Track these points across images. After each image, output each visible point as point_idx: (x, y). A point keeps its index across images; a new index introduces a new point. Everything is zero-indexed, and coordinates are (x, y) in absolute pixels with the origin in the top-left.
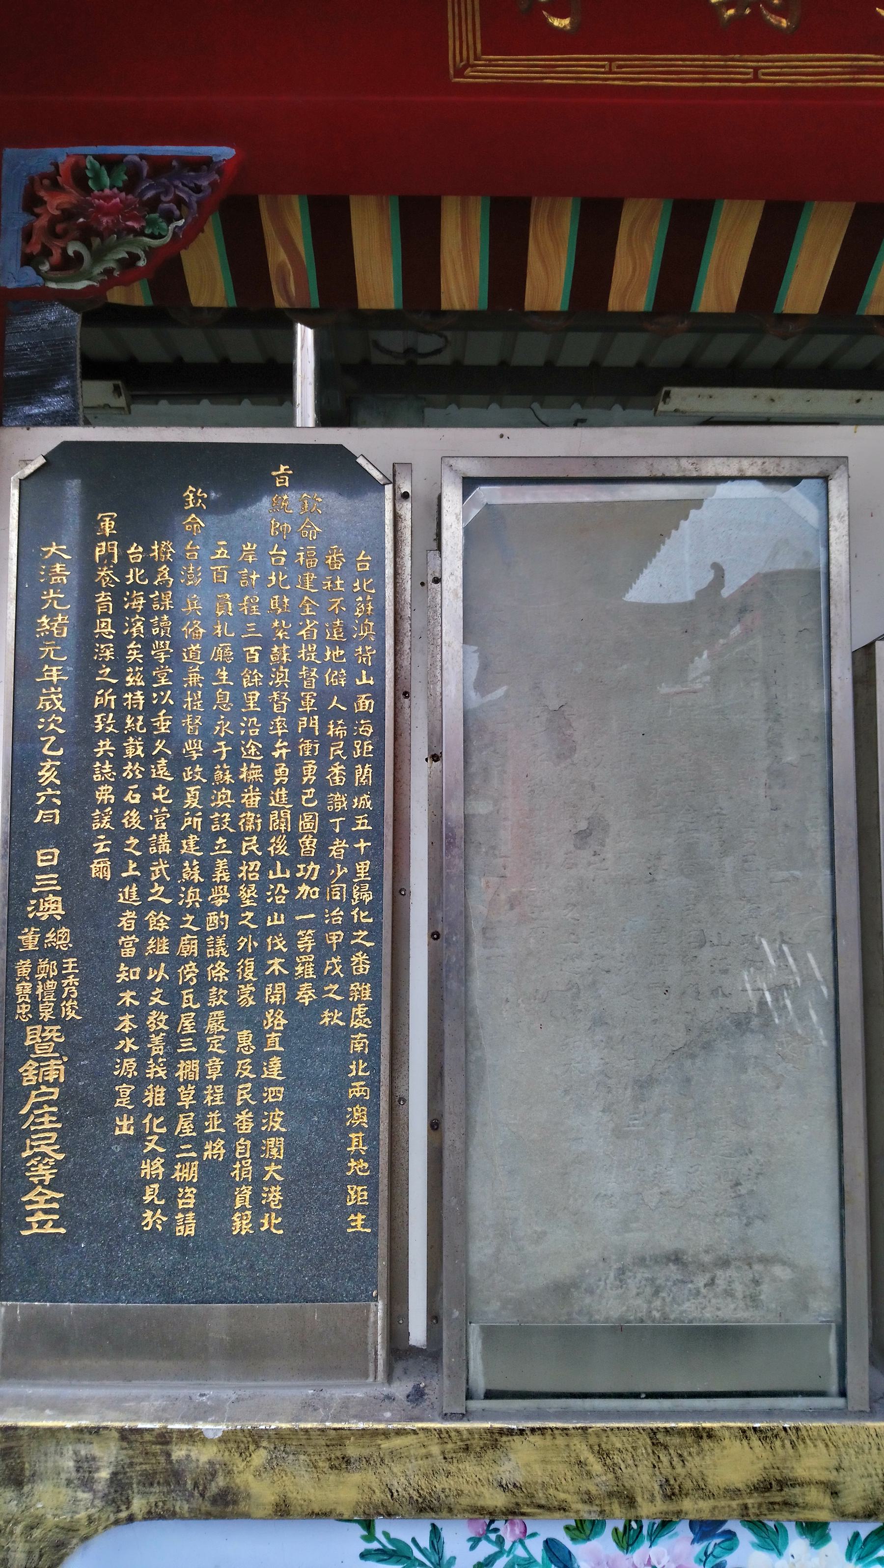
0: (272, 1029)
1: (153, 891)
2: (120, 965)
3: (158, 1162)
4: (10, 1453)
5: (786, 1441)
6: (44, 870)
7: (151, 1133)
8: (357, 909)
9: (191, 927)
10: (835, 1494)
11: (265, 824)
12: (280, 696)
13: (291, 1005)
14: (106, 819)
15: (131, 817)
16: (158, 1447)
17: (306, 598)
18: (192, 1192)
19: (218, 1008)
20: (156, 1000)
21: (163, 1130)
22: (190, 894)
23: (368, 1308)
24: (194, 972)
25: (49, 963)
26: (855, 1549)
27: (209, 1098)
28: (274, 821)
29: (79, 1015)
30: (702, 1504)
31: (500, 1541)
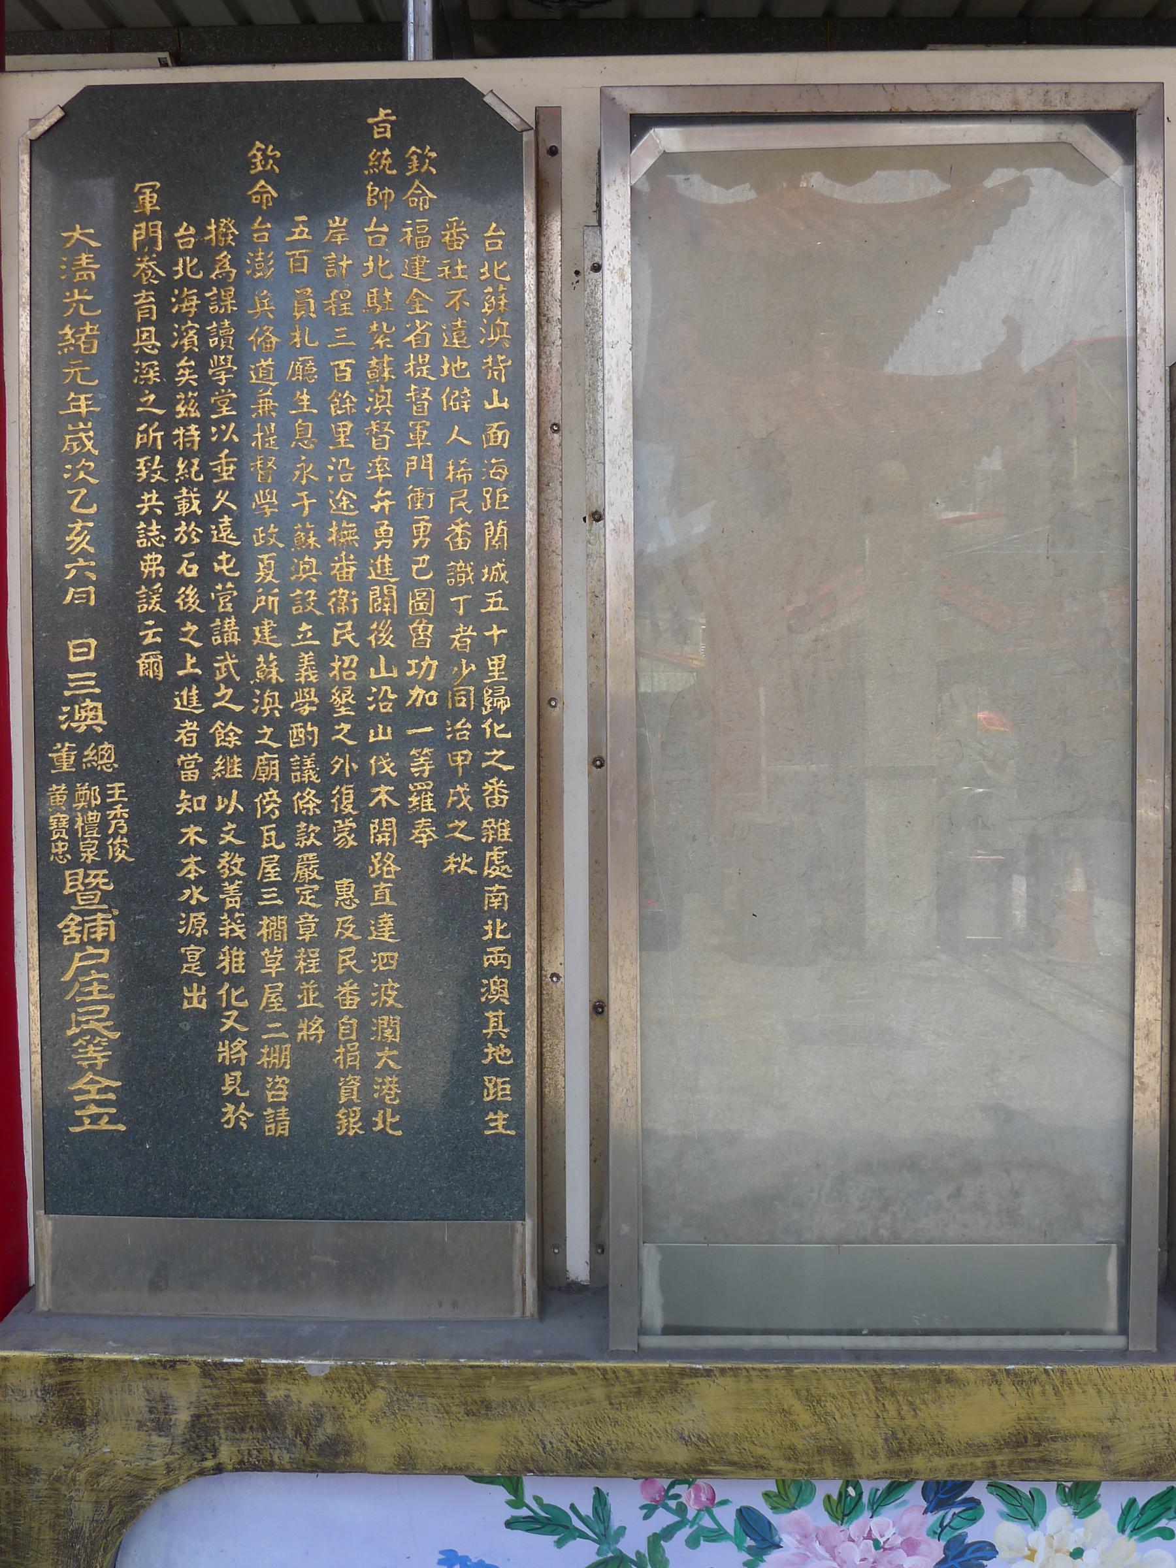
0: (380, 877)
1: (218, 695)
2: (180, 793)
3: (240, 1044)
4: (68, 1389)
5: (1047, 1387)
6: (78, 667)
7: (229, 1007)
8: (490, 720)
9: (270, 743)
10: (1106, 1449)
11: (363, 605)
12: (381, 427)
13: (404, 847)
14: (155, 598)
15: (187, 596)
16: (249, 1385)
17: (415, 290)
18: (283, 1082)
19: (308, 849)
20: (229, 838)
21: (245, 1004)
22: (266, 699)
23: (513, 1230)
24: (275, 802)
25: (89, 789)
26: (1129, 1519)
27: (302, 964)
28: (375, 600)
29: (130, 856)
30: (937, 1462)
31: (682, 1510)
